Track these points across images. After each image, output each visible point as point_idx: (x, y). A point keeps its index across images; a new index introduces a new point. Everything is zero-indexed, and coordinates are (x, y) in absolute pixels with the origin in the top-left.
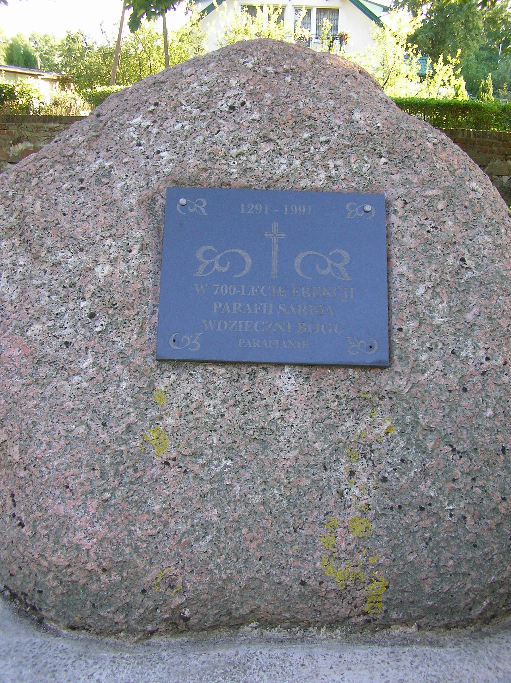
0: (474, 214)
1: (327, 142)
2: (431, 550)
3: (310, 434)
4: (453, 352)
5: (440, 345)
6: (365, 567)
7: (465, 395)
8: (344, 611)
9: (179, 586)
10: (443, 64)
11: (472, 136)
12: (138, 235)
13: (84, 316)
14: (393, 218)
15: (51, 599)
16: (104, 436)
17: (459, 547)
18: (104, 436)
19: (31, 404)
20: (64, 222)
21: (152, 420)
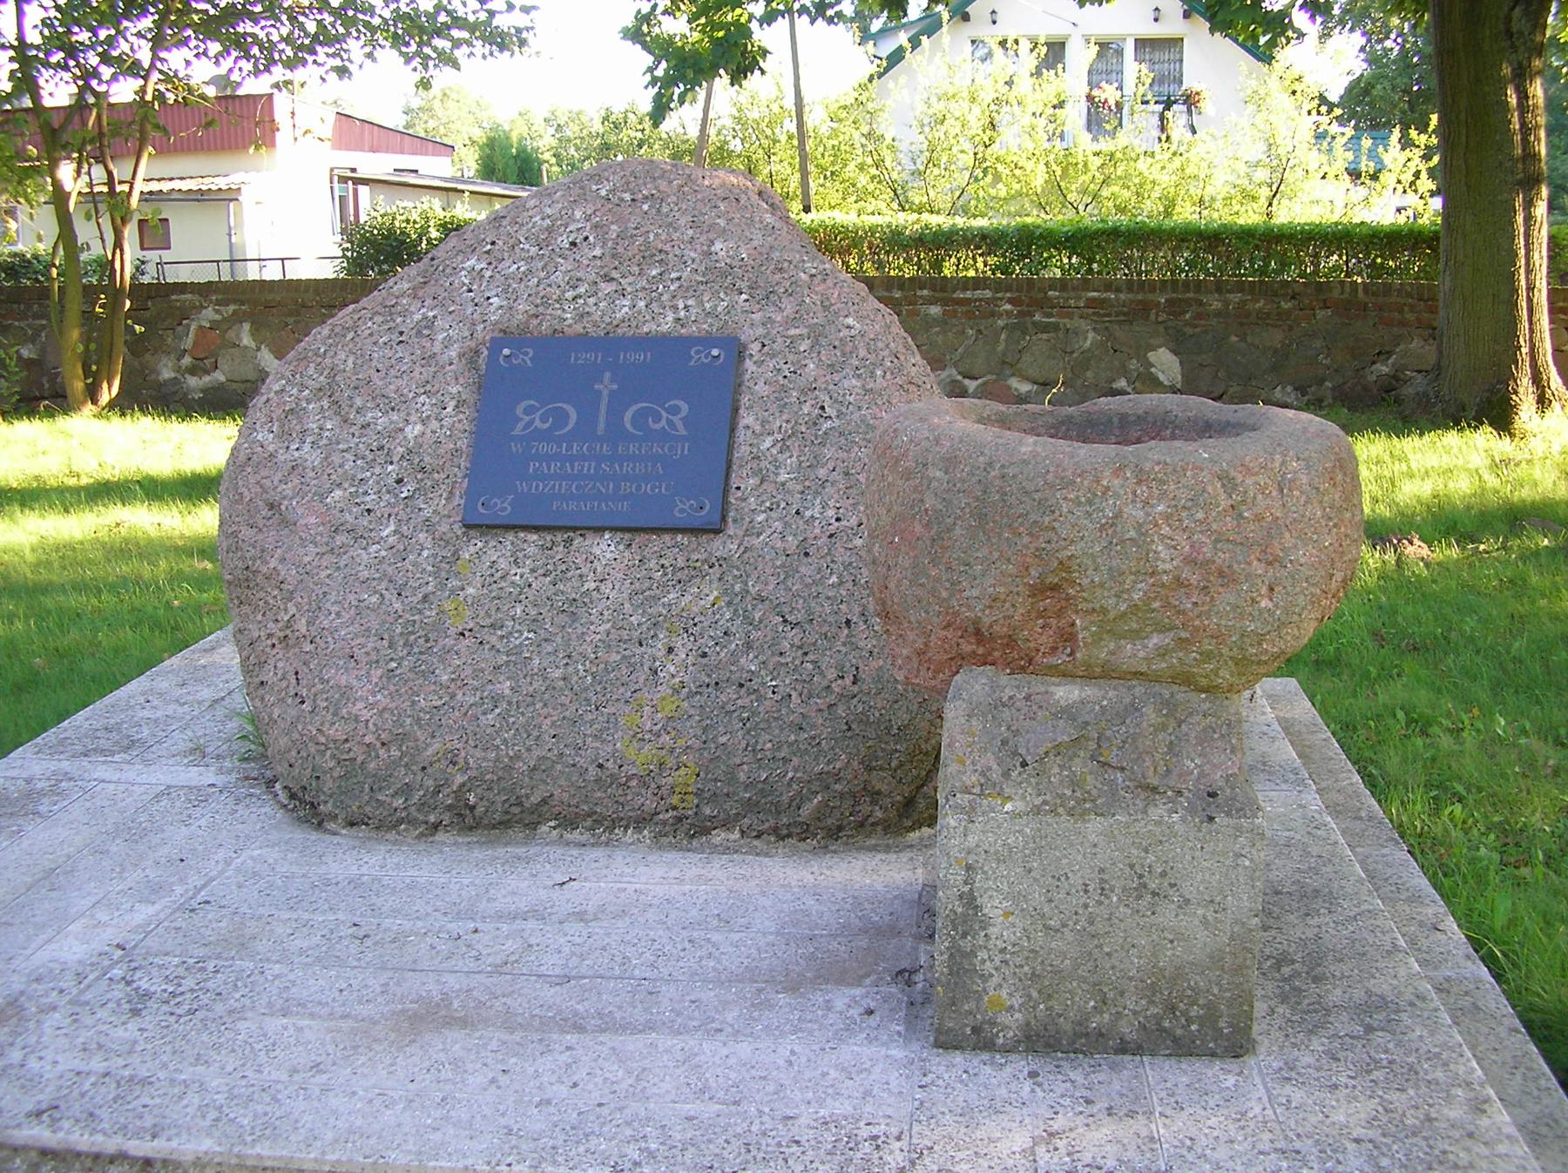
0: (844, 355)
1: (679, 279)
2: (748, 732)
3: (627, 605)
4: (798, 513)
5: (783, 505)
6: (672, 750)
7: (805, 560)
8: (650, 805)
9: (461, 761)
10: (1399, 146)
11: (1361, 294)
12: (454, 391)
13: (391, 481)
14: (748, 364)
15: (329, 785)
16: (397, 606)
17: (782, 729)
18: (397, 606)
19: (323, 574)
20: (377, 380)
21: (452, 591)
